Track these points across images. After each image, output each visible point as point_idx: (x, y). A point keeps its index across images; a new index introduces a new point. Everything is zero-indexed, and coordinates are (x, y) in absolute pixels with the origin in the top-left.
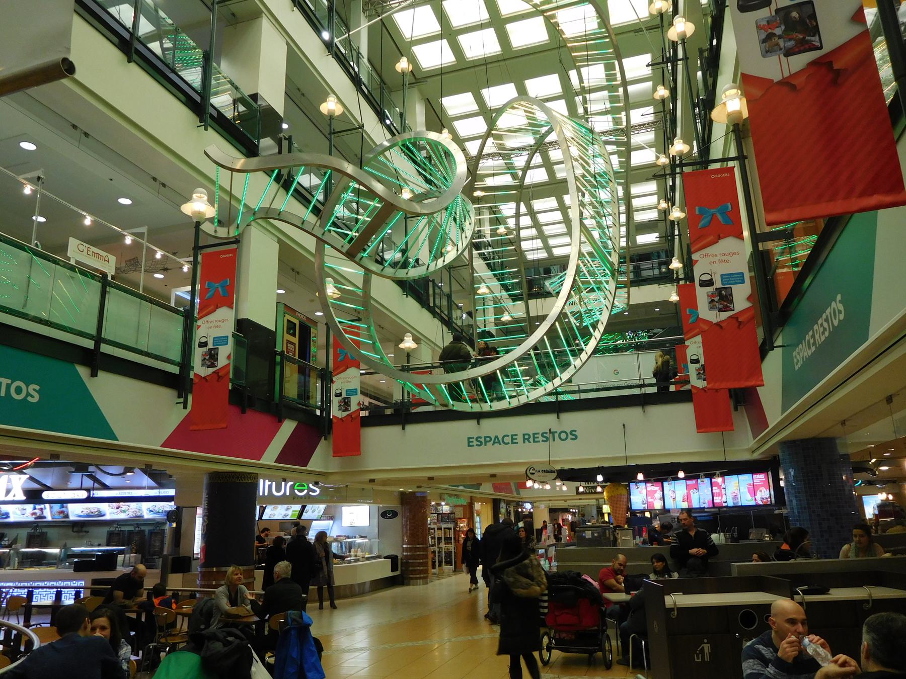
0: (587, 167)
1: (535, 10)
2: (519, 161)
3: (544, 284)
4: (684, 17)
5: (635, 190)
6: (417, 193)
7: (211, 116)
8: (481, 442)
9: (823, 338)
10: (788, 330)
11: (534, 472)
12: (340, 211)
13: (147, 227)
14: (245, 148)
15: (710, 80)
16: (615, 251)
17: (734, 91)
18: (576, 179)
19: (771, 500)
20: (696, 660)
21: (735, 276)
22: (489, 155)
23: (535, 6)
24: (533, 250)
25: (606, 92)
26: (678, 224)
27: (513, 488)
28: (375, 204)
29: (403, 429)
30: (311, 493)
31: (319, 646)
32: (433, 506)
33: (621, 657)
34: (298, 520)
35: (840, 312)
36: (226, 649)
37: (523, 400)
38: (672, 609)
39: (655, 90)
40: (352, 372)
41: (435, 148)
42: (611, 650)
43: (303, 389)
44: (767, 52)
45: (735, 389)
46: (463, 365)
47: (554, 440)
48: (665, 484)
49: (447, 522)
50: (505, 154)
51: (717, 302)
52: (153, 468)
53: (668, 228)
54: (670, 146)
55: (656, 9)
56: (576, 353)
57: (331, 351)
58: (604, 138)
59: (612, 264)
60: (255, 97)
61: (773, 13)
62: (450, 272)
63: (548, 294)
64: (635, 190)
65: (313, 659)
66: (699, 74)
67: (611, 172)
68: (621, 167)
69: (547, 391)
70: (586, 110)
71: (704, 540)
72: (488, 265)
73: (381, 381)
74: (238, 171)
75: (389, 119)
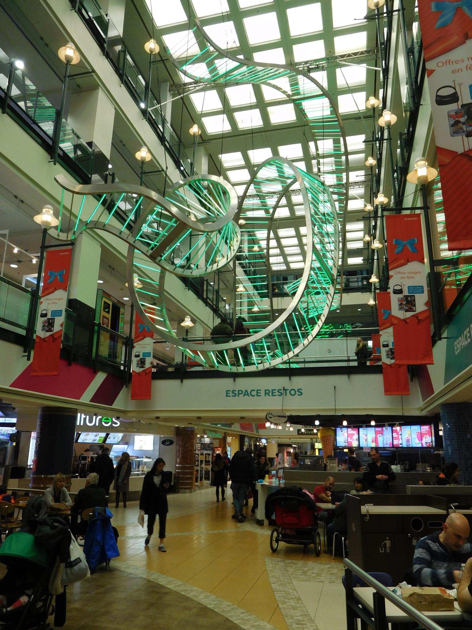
0: (316, 210)
1: (288, 98)
2: (271, 202)
3: (283, 287)
4: (390, 111)
5: (349, 227)
6: (199, 218)
7: (59, 155)
8: (236, 394)
10: (451, 327)
11: (272, 416)
12: (145, 228)
13: (8, 230)
14: (81, 179)
15: (406, 155)
16: (335, 266)
17: (423, 162)
18: (312, 216)
19: (432, 444)
20: (381, 552)
21: (418, 288)
22: (250, 196)
23: (288, 96)
24: (277, 264)
25: (333, 158)
26: (377, 252)
27: (254, 427)
28: (172, 223)
29: (182, 382)
30: (113, 425)
31: (116, 533)
32: (198, 438)
33: (326, 548)
34: (103, 444)
36: (53, 531)
37: (267, 365)
38: (365, 515)
39: (366, 159)
40: (148, 340)
41: (216, 187)
42: (320, 543)
43: (112, 351)
44: (454, 133)
45: (412, 366)
46: (227, 339)
47: (286, 395)
48: (361, 430)
49: (207, 450)
50: (261, 196)
51: (404, 305)
52: (3, 402)
53: (370, 254)
54: (375, 198)
56: (305, 335)
57: (134, 325)
58: (331, 190)
59: (332, 275)
60: (90, 144)
61: (460, 107)
62: (219, 275)
63: (286, 295)
64: (349, 227)
65: (112, 542)
66: (399, 150)
67: (335, 212)
68: (340, 210)
69: (284, 360)
70: (319, 169)
71: (386, 470)
72: (245, 272)
73: (167, 348)
74: (78, 193)
75: (183, 167)
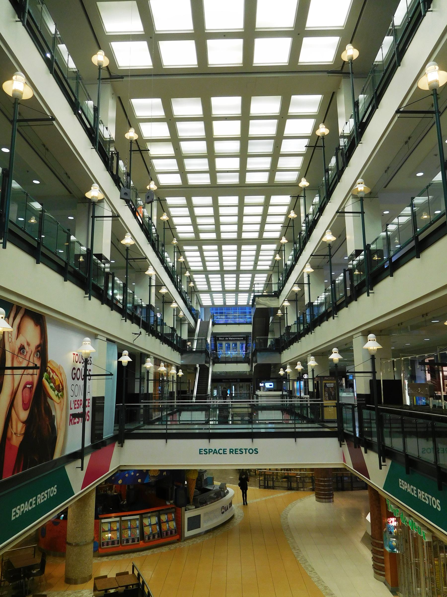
8: (207, 452)
9: (42, 501)
35: (55, 491)
55: (348, 56)
